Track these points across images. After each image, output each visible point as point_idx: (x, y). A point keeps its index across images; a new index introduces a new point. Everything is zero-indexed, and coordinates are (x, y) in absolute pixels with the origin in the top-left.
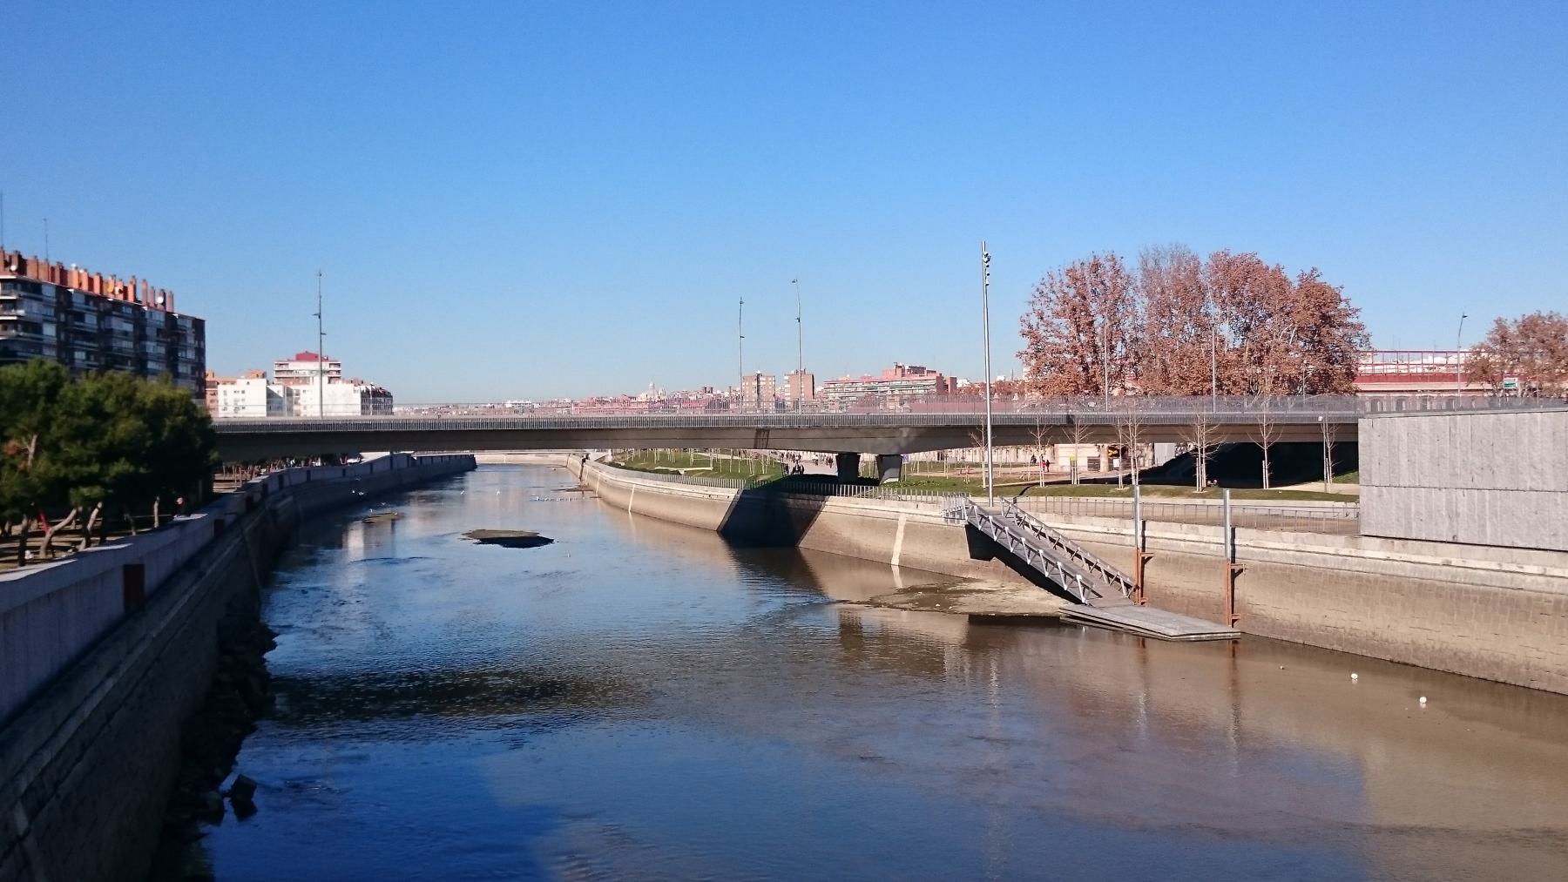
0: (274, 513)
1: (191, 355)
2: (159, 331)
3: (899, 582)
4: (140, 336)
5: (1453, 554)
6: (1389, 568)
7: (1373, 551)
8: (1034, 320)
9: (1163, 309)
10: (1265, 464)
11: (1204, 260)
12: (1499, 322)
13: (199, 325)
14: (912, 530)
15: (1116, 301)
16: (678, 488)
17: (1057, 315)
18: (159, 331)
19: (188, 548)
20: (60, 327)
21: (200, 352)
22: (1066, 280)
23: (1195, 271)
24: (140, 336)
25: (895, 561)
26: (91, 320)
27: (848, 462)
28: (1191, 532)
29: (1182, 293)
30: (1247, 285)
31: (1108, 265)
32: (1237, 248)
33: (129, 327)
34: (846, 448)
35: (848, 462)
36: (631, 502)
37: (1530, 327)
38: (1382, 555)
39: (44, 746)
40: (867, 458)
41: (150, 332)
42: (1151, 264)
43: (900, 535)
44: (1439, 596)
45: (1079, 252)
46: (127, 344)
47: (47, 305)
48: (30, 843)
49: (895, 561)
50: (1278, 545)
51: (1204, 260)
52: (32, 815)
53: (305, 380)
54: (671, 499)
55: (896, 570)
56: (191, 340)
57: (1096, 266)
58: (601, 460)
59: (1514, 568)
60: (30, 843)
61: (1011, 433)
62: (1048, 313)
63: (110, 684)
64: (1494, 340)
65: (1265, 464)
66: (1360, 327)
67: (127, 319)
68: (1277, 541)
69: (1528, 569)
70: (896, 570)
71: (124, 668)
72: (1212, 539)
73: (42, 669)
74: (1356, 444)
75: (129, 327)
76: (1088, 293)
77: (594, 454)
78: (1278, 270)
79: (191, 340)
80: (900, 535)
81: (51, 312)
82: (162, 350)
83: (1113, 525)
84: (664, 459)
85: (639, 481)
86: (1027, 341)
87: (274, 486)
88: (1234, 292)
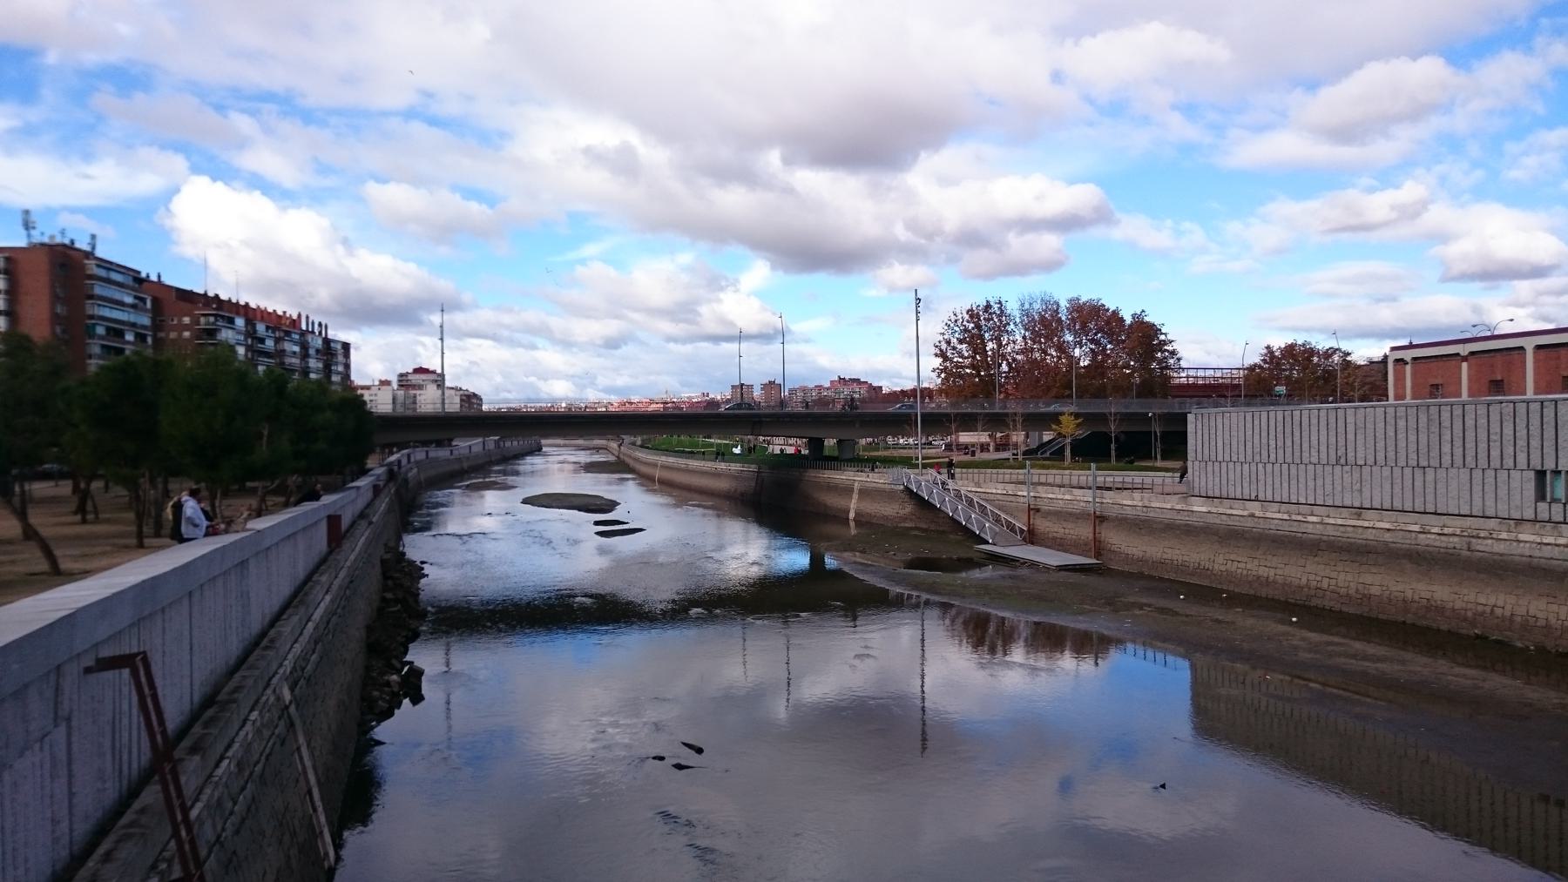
0: (406, 481)
1: (341, 368)
2: (318, 351)
3: (853, 531)
4: (305, 355)
5: (1255, 508)
6: (1211, 520)
7: (1199, 507)
8: (944, 346)
9: (1036, 337)
10: (1113, 446)
11: (1064, 304)
12: (1268, 347)
13: (346, 347)
14: (865, 493)
15: (1001, 330)
16: (694, 464)
17: (961, 341)
18: (318, 351)
19: (360, 504)
20: (248, 348)
21: (347, 366)
22: (967, 317)
23: (1057, 311)
24: (305, 355)
25: (852, 515)
26: (270, 343)
27: (816, 444)
28: (1070, 490)
29: (1045, 325)
30: (1091, 317)
31: (996, 307)
32: (1087, 294)
33: (296, 349)
34: (815, 434)
35: (816, 444)
36: (657, 473)
37: (1290, 350)
38: (1204, 509)
39: (296, 641)
40: (830, 442)
41: (312, 352)
42: (1027, 306)
43: (855, 496)
44: (1271, 746)
45: (977, 295)
46: (295, 361)
47: (239, 333)
48: (292, 709)
49: (852, 515)
50: (1130, 502)
51: (1064, 304)
52: (292, 690)
53: (420, 387)
54: (687, 471)
55: (852, 524)
56: (341, 358)
57: (988, 306)
58: (634, 444)
59: (1300, 518)
60: (292, 709)
61: (935, 423)
62: (954, 341)
63: (328, 598)
64: (1264, 361)
65: (1113, 446)
66: (1173, 353)
67: (295, 343)
68: (1142, 493)
69: (1311, 519)
70: (852, 524)
71: (335, 587)
72: (1083, 499)
73: (285, 589)
74: (1185, 433)
75: (296, 349)
76: (981, 325)
77: (627, 439)
78: (1115, 313)
79: (341, 358)
80: (855, 496)
81: (242, 338)
82: (320, 365)
83: (1010, 489)
84: (680, 443)
85: (664, 458)
86: (940, 360)
87: (404, 462)
88: (1084, 326)
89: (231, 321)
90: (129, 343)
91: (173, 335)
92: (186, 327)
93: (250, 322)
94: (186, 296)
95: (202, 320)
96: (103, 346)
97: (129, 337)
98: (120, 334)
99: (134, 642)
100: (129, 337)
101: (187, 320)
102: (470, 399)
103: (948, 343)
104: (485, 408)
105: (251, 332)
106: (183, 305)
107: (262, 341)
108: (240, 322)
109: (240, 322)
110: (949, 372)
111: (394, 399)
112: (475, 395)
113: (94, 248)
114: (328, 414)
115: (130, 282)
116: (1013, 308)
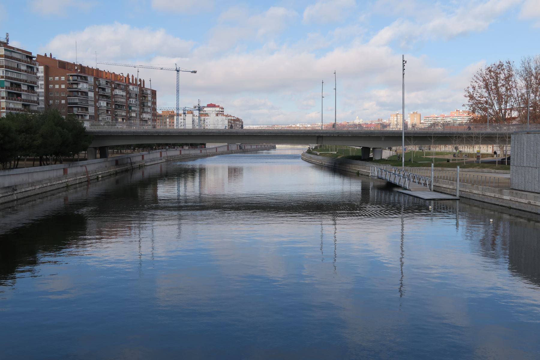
1: (150, 104)
33: (124, 94)
89: (86, 78)
90: (23, 91)
91: (57, 86)
92: (63, 82)
93: (96, 79)
94: (63, 65)
95: (71, 78)
96: (9, 93)
97: (24, 88)
98: (19, 86)
99: (329, 103)
100: (24, 88)
101: (63, 78)
102: (235, 122)
103: (474, 88)
104: (245, 127)
105: (97, 86)
106: (62, 70)
107: (104, 89)
108: (91, 79)
109: (91, 79)
110: (476, 104)
111: (193, 121)
112: (238, 120)
113: (8, 41)
114: (537, 97)
115: (24, 58)
116: (517, 66)
